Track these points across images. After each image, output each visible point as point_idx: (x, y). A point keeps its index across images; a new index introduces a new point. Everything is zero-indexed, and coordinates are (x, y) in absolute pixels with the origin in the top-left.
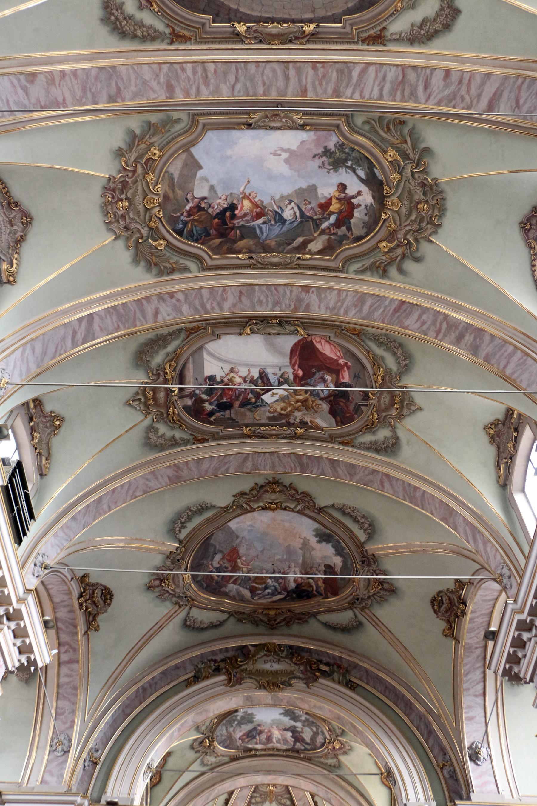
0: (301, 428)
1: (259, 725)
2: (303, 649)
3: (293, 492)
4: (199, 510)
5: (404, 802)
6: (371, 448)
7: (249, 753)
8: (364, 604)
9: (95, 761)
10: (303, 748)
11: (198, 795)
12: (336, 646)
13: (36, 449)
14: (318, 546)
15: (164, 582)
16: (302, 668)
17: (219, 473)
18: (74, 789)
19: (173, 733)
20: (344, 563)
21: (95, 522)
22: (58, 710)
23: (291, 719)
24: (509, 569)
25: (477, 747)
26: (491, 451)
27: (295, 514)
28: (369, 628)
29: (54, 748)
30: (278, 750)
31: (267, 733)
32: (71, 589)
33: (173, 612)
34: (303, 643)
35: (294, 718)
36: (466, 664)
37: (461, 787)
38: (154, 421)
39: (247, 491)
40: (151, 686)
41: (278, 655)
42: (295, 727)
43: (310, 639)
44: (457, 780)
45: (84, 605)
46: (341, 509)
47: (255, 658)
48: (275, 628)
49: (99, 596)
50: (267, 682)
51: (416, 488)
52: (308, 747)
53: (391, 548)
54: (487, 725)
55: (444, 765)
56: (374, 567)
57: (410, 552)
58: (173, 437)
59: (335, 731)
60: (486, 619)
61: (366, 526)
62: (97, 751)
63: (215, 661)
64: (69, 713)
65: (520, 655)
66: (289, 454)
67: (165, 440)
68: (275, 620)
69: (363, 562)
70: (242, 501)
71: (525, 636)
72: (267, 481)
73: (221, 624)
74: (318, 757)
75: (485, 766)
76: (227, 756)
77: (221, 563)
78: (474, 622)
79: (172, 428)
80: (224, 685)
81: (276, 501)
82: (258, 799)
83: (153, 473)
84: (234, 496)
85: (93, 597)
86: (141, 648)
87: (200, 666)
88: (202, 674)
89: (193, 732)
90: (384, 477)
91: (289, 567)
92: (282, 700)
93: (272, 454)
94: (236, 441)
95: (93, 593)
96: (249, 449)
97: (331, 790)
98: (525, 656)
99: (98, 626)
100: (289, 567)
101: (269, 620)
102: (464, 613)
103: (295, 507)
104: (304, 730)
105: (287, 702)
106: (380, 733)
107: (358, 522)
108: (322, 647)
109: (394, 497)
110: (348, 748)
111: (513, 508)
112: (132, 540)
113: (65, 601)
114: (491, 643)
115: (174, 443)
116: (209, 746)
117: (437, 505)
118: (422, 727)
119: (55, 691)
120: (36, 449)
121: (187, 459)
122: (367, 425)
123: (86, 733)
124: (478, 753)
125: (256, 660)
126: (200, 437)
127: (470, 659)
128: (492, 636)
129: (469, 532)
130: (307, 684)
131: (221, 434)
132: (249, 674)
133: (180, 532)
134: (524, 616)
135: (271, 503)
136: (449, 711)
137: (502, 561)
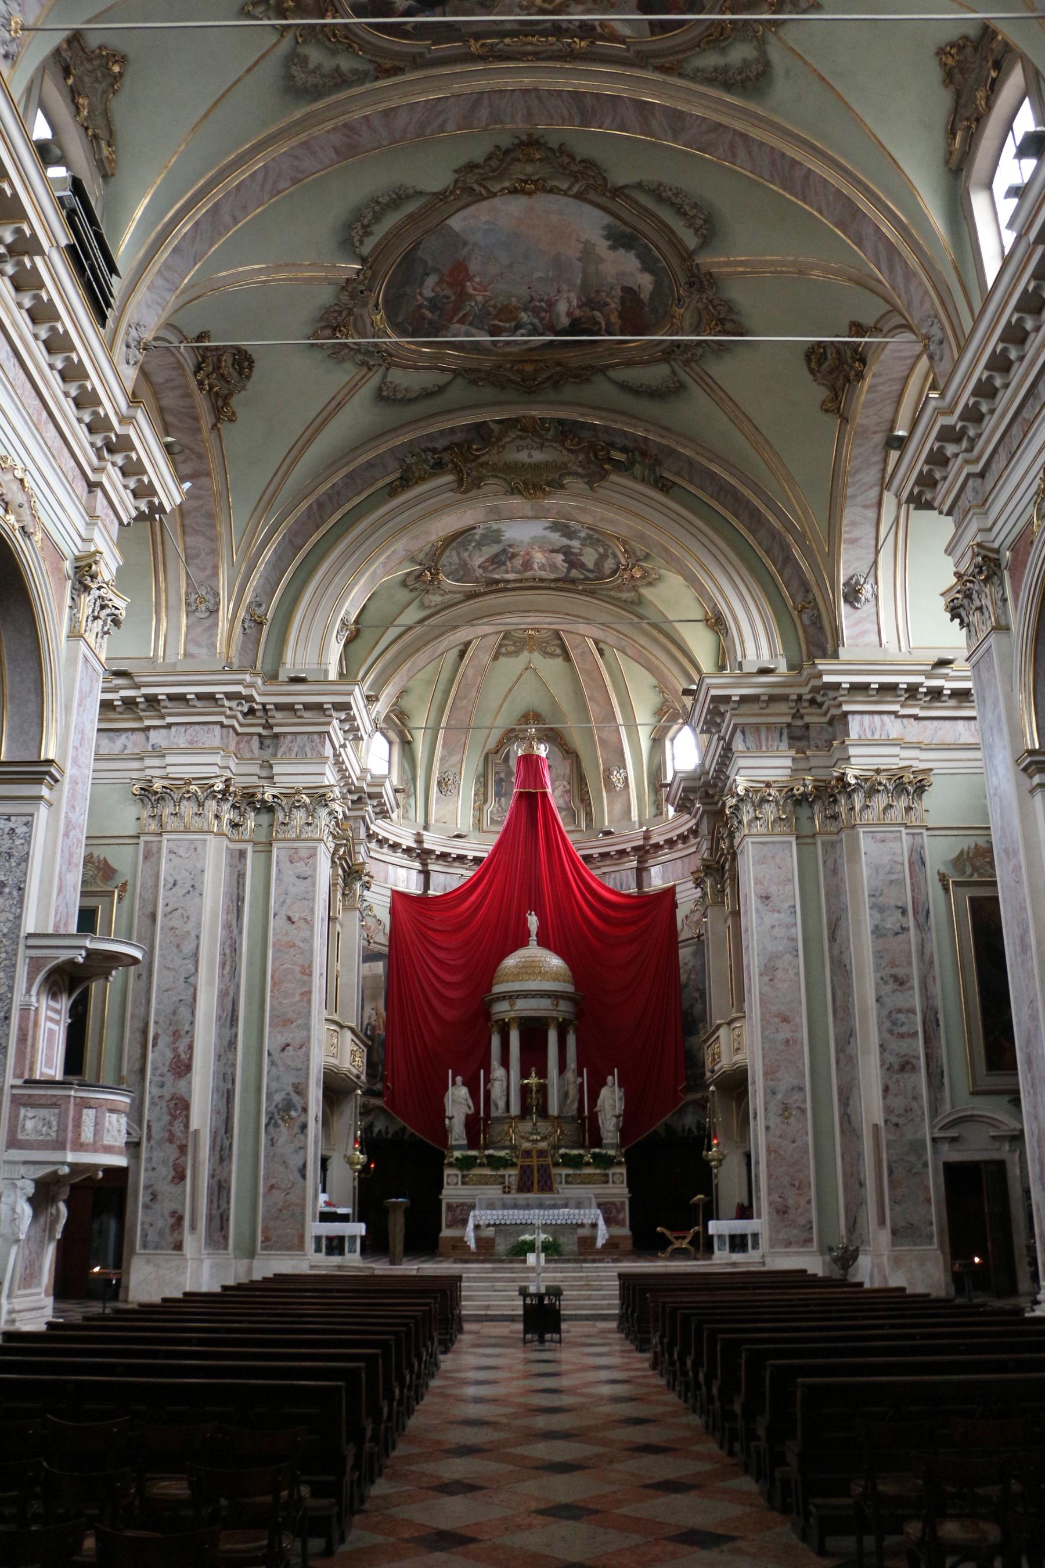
0: (581, 39)
1: (510, 546)
2: (583, 425)
3: (566, 160)
4: (394, 201)
5: (739, 659)
6: (715, 79)
7: (495, 586)
8: (689, 355)
9: (259, 620)
10: (582, 577)
11: (418, 650)
12: (639, 419)
13: (86, 129)
14: (609, 256)
15: (340, 331)
16: (581, 457)
17: (428, 131)
18: (235, 661)
19: (375, 571)
20: (658, 284)
21: (213, 249)
22: (188, 551)
23: (564, 535)
24: (943, 329)
25: (857, 583)
26: (942, 100)
27: (570, 200)
28: (696, 392)
29: (194, 608)
30: (542, 580)
31: (524, 556)
32: (182, 360)
33: (358, 378)
34: (582, 415)
35: (569, 533)
36: (856, 458)
37: (826, 638)
38: (297, 43)
39: (481, 161)
40: (330, 498)
41: (540, 436)
42: (569, 547)
43: (594, 408)
44: (821, 629)
45: (206, 382)
46: (653, 191)
47: (500, 444)
48: (535, 391)
49: (229, 365)
50: (524, 482)
51: (794, 163)
52: (591, 575)
53: (741, 263)
54: (877, 552)
55: (803, 607)
56: (710, 294)
57: (776, 272)
58: (337, 69)
59: (634, 553)
60: (897, 387)
61: (699, 222)
62: (260, 605)
63: (434, 451)
64: (207, 554)
65: (938, 475)
66: (559, 93)
67: (323, 76)
68: (534, 380)
69: (691, 285)
70: (471, 180)
71: (950, 449)
72: (516, 141)
73: (441, 389)
74: (606, 589)
75: (866, 609)
76: (460, 593)
77: (438, 289)
78: (876, 391)
79: (334, 53)
80: (451, 490)
81: (534, 178)
82: (511, 648)
83: (305, 144)
84: (456, 171)
85: (219, 367)
86: (310, 441)
87: (410, 460)
88: (413, 473)
89: (406, 564)
90: (737, 138)
91: (559, 291)
92: (549, 510)
93: (525, 92)
94: (458, 69)
95: (219, 361)
96: (483, 84)
97: (626, 636)
98: (945, 478)
99: (234, 413)
100: (559, 291)
101: (523, 380)
102: (860, 376)
103: (570, 188)
104: (584, 552)
105: (558, 514)
106: (708, 560)
107: (685, 214)
108: (615, 421)
109: (752, 176)
110: (654, 576)
111: (965, 217)
112: (279, 268)
113: (172, 380)
114: (894, 455)
115: (340, 80)
116: (430, 581)
117: (831, 198)
118: (776, 550)
119: (178, 524)
120: (86, 129)
121: (368, 112)
122: (711, 35)
123: (238, 582)
124: (858, 591)
125: (504, 447)
126: (388, 64)
127: (862, 449)
128: (901, 443)
129: (883, 255)
130: (590, 484)
131: (428, 56)
132: (493, 470)
133: (361, 242)
134: (952, 420)
135: (526, 182)
136: (820, 529)
137: (933, 312)
